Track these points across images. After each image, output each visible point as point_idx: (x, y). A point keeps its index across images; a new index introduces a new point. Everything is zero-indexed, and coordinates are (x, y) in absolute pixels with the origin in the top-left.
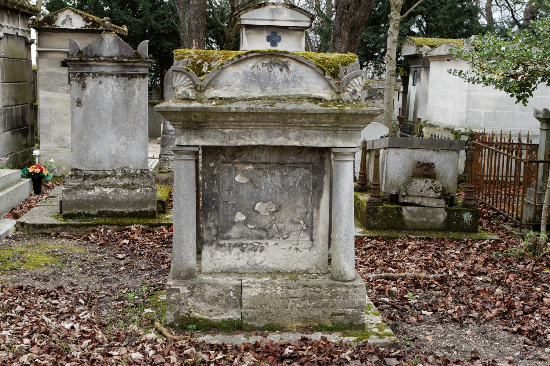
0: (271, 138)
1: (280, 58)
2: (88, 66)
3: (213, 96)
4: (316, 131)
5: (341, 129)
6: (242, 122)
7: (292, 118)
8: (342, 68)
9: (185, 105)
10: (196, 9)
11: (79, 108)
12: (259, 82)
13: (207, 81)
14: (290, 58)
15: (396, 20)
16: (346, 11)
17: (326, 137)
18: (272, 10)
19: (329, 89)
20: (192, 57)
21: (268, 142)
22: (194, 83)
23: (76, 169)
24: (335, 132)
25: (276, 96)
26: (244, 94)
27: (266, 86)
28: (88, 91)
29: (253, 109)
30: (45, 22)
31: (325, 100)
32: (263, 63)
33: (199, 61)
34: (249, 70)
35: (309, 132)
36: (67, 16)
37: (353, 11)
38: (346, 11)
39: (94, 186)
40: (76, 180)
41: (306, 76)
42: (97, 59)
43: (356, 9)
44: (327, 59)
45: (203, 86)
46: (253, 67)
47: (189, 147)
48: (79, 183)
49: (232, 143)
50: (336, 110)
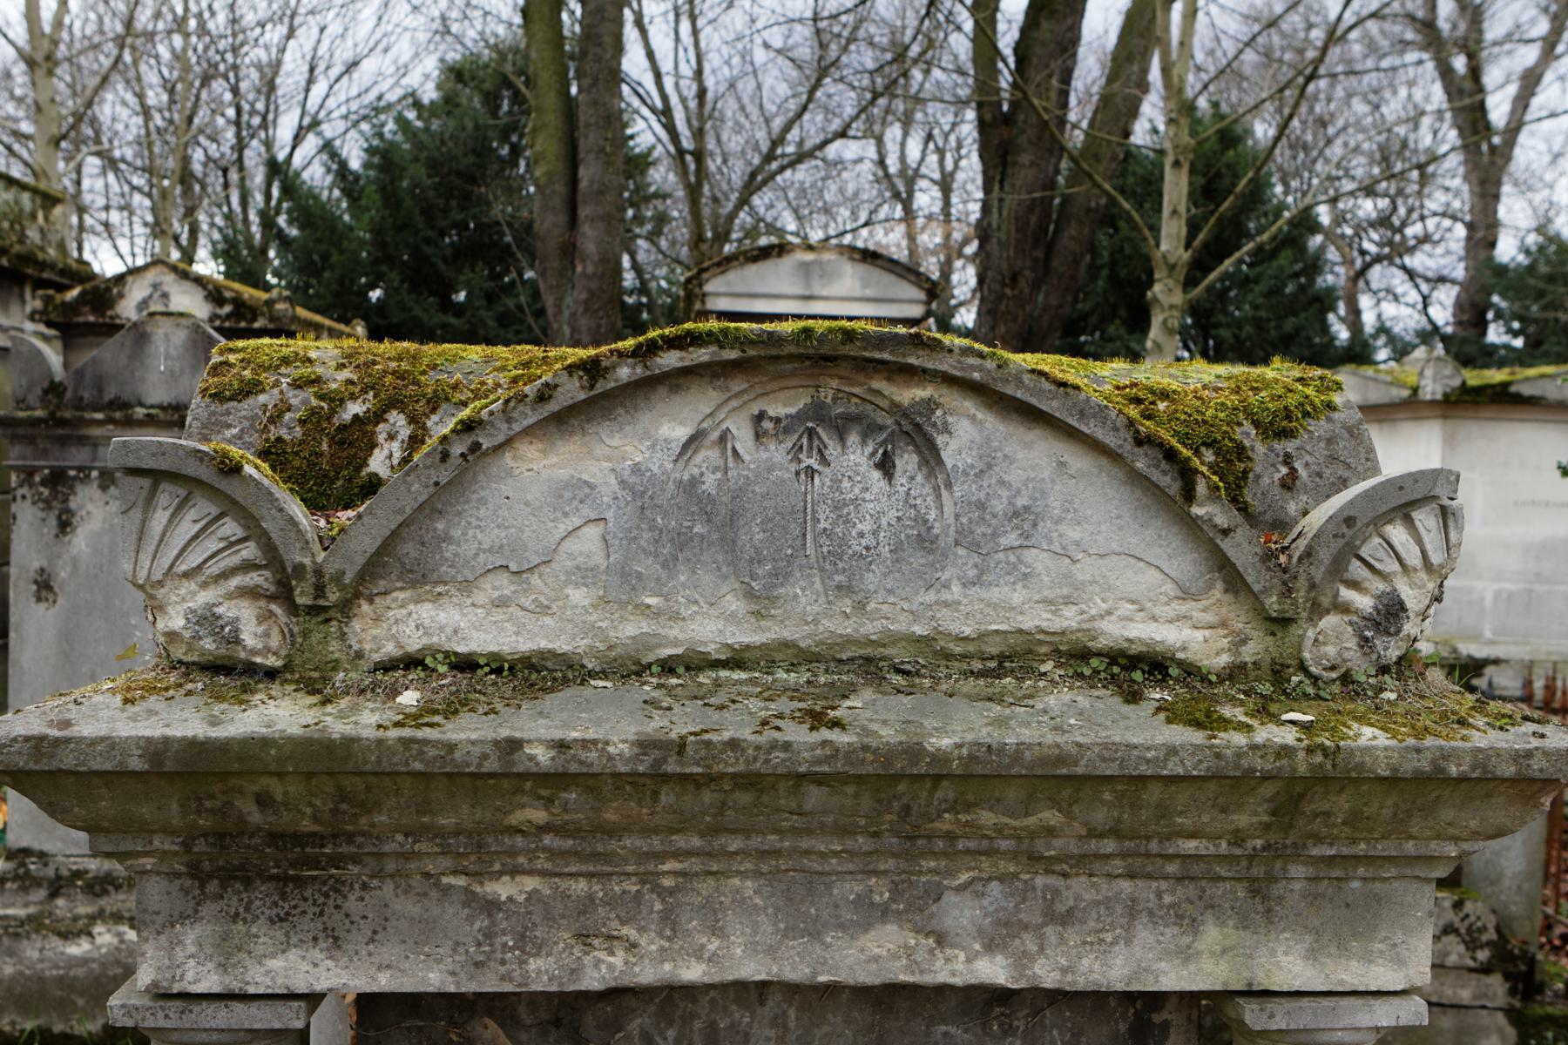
0: (816, 935)
1: (879, 384)
2: (82, 441)
3: (414, 644)
4: (1126, 886)
5: (1298, 870)
6: (613, 832)
7: (969, 807)
8: (1260, 449)
9: (185, 720)
10: (593, 285)
11: (42, 606)
12: (729, 544)
13: (364, 544)
14: (950, 380)
15: (1172, 307)
16: (1008, 291)
17: (1194, 925)
18: (805, 267)
19: (1217, 592)
20: (317, 381)
21: (794, 967)
22: (272, 557)
23: (26, 852)
24: (1258, 889)
25: (849, 641)
26: (630, 629)
27: (781, 575)
28: (80, 541)
29: (681, 746)
30: (85, 303)
31: (1191, 671)
32: (760, 417)
33: (355, 408)
34: (659, 463)
35: (1080, 889)
36: (155, 286)
37: (1027, 290)
38: (1008, 291)
39: (93, 919)
40: (21, 899)
41: (1055, 505)
42: (118, 415)
43: (1036, 286)
44: (1165, 395)
45: (338, 577)
46: (693, 441)
47: (238, 1007)
48: (32, 910)
49: (541, 973)
50: (1285, 751)
